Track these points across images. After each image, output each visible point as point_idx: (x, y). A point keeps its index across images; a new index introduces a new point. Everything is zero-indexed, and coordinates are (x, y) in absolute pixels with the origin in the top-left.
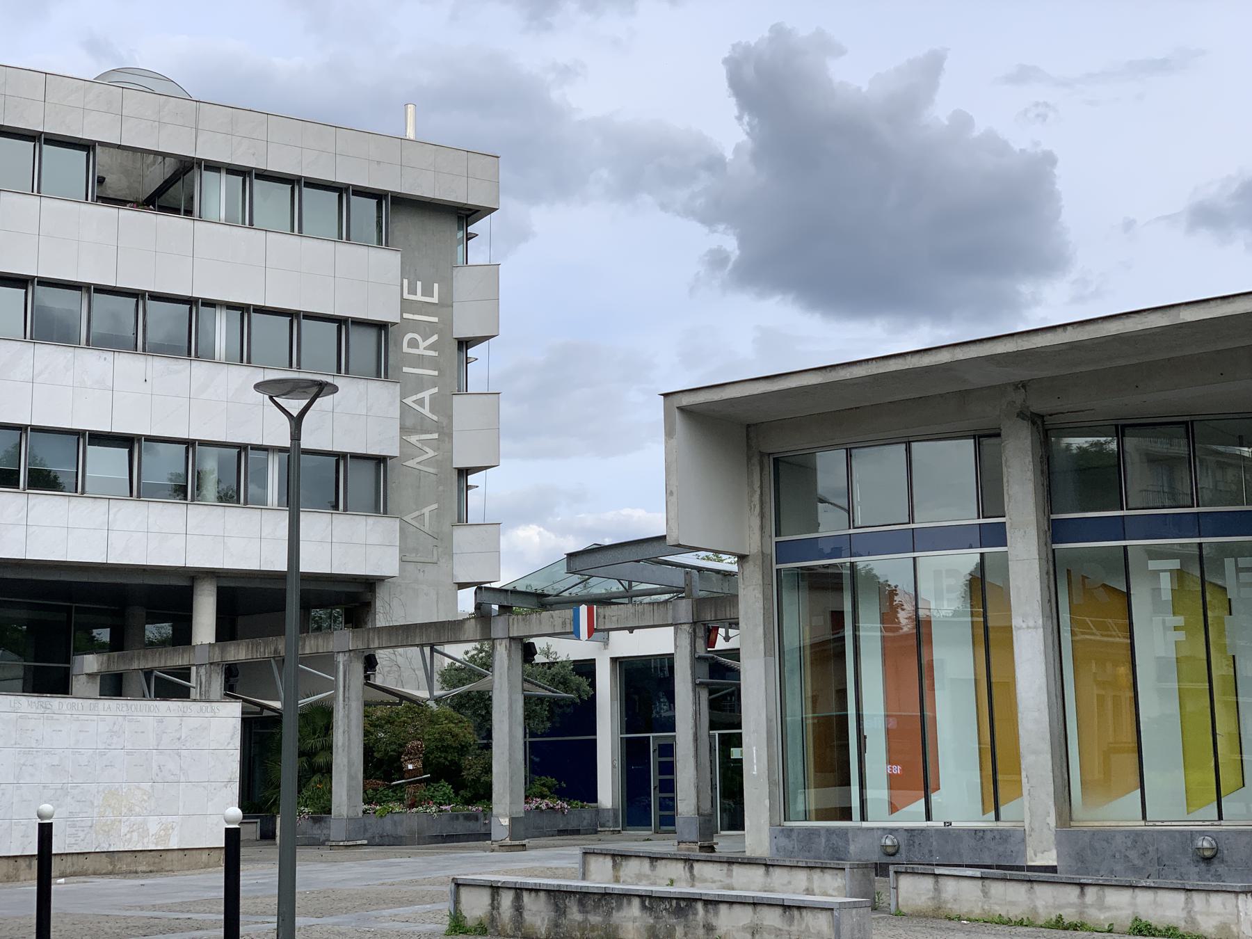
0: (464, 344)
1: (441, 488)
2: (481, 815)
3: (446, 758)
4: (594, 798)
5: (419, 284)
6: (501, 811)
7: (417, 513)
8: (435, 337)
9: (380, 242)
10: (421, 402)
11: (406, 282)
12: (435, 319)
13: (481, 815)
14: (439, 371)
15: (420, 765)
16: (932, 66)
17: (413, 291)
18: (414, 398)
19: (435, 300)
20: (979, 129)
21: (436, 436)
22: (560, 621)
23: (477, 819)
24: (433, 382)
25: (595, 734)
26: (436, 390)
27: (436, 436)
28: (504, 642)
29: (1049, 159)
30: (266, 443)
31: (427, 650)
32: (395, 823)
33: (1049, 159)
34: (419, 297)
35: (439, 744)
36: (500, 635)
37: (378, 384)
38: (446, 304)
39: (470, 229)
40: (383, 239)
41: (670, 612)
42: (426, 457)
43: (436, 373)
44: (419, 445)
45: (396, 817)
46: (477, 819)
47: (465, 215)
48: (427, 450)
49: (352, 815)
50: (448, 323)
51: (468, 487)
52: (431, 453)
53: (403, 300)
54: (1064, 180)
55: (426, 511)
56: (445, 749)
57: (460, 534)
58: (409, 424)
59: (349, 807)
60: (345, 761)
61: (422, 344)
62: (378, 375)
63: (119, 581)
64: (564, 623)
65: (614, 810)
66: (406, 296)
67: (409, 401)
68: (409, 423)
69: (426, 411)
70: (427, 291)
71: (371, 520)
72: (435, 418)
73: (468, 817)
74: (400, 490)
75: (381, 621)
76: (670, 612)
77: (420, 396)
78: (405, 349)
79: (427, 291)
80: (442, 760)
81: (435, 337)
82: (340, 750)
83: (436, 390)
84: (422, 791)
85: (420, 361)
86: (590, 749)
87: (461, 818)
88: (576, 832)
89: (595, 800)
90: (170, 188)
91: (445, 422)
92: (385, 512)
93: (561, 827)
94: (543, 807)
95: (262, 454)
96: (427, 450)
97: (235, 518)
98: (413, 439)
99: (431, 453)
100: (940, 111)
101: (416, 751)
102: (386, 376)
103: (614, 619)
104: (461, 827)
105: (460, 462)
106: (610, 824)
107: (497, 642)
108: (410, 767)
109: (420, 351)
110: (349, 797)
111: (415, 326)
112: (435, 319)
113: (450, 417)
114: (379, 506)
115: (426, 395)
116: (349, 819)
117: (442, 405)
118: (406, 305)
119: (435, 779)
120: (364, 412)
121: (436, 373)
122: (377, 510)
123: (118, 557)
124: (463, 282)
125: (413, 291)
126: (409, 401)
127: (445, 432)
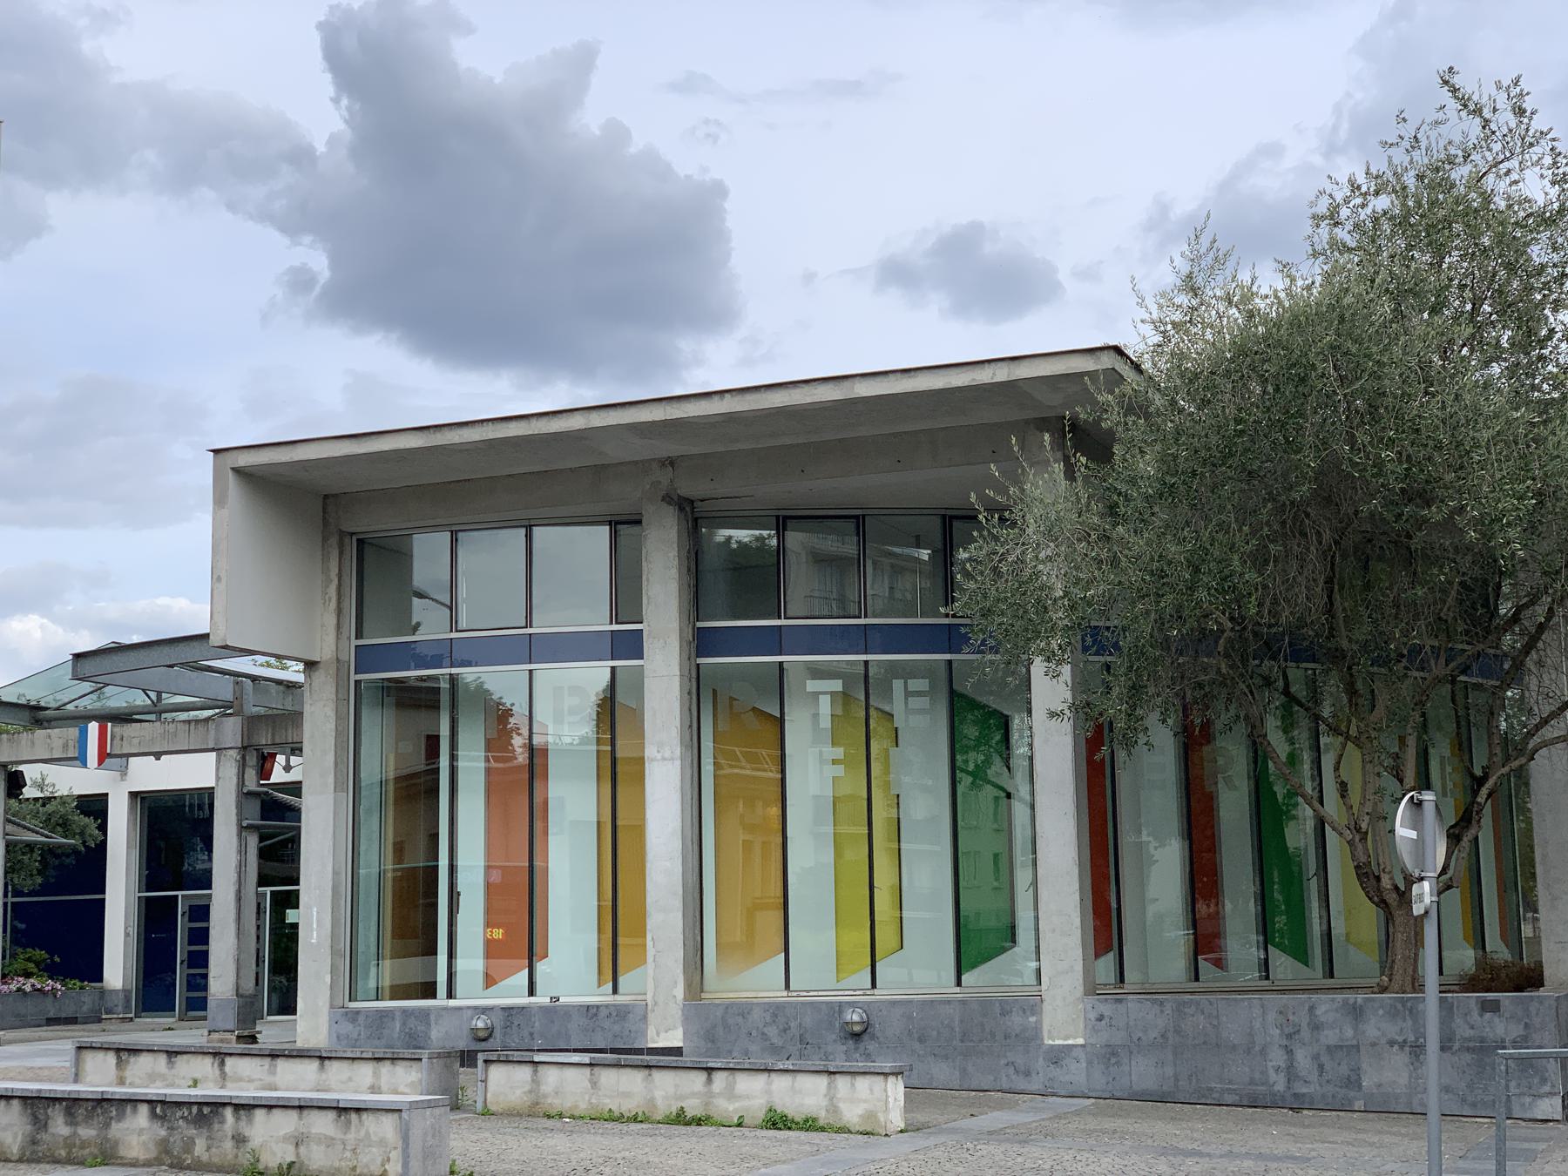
4: (98, 975)
16: (582, 60)
20: (636, 145)
22: (61, 742)
64: (65, 746)
65: (126, 992)
89: (100, 979)
93: (51, 1015)
100: (590, 118)
103: (136, 741)
106: (120, 1009)
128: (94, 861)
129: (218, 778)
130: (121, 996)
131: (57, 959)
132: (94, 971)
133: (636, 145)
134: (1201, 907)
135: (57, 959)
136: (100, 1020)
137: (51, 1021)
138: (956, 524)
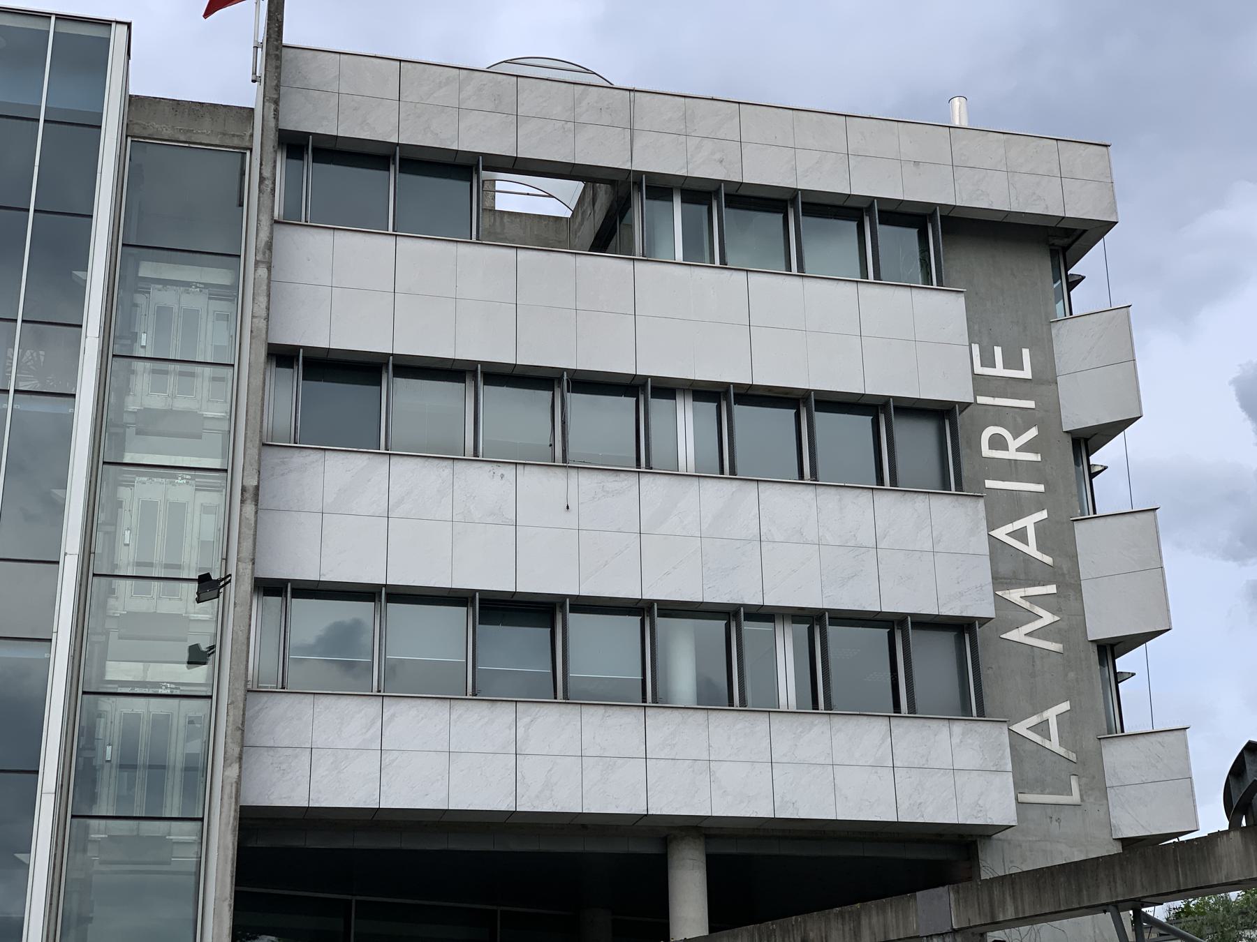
0: (1110, 649)
1: (1072, 675)
5: (998, 351)
7: (1034, 720)
8: (1033, 433)
9: (927, 279)
10: (1021, 535)
11: (976, 348)
12: (1031, 404)
17: (988, 361)
18: (1010, 528)
19: (1027, 373)
21: (1052, 589)
24: (1036, 502)
26: (1043, 515)
27: (1052, 589)
30: (771, 600)
34: (999, 370)
37: (947, 500)
38: (1045, 380)
39: (1094, 459)
40: (930, 275)
42: (1038, 624)
43: (1041, 488)
44: (1026, 605)
47: (1061, 242)
48: (1038, 610)
51: (1119, 677)
52: (1047, 618)
53: (976, 376)
55: (1051, 714)
57: (1115, 756)
58: (1007, 569)
61: (1013, 444)
62: (946, 485)
63: (544, 847)
66: (979, 370)
67: (1001, 533)
68: (1005, 568)
69: (1031, 549)
70: (1013, 361)
71: (958, 728)
72: (1048, 560)
74: (1002, 682)
75: (985, 875)
77: (1018, 525)
78: (986, 452)
79: (1013, 361)
81: (1033, 433)
83: (1043, 515)
85: (1011, 470)
90: (615, 209)
91: (1065, 566)
92: (981, 712)
95: (765, 627)
96: (1038, 610)
97: (730, 732)
98: (1015, 595)
99: (1047, 618)
102: (959, 486)
105: (1100, 630)
109: (1011, 454)
112: (1031, 404)
113: (1074, 558)
114: (971, 702)
115: (1029, 522)
117: (1057, 537)
118: (981, 384)
120: (928, 546)
121: (1041, 488)
122: (965, 710)
123: (535, 801)
124: (1070, 343)
125: (988, 361)
126: (1001, 533)
127: (1068, 581)
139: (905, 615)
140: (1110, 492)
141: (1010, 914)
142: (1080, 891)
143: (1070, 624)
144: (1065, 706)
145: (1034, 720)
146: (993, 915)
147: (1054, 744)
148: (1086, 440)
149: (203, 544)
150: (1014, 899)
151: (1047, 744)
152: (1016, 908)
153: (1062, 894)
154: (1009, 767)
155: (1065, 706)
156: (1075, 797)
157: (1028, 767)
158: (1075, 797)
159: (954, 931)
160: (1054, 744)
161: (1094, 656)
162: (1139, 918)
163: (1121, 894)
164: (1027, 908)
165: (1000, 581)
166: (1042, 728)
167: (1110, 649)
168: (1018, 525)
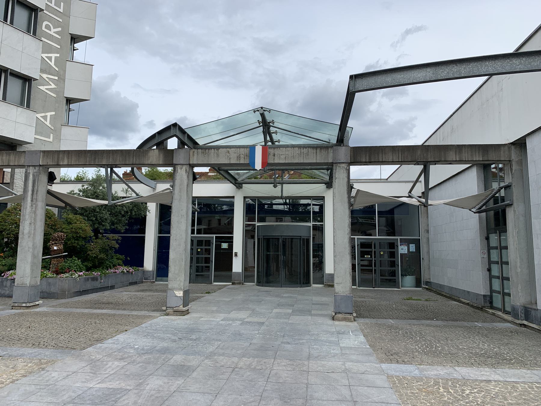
0: (75, 39)
1: (57, 105)
2: (99, 278)
3: (78, 244)
4: (142, 265)
6: (176, 286)
7: (43, 114)
8: (60, 29)
10: (50, 58)
12: (61, 20)
13: (99, 278)
14: (61, 46)
15: (61, 247)
16: (114, 78)
20: (122, 96)
21: (56, 78)
22: (236, 155)
23: (97, 280)
24: (56, 51)
25: (144, 233)
27: (56, 78)
28: (184, 167)
29: (134, 106)
31: (109, 169)
32: (49, 284)
33: (134, 106)
34: (53, 5)
35: (75, 235)
36: (182, 162)
38: (66, 15)
41: (331, 155)
43: (59, 47)
44: (47, 80)
45: (50, 280)
46: (97, 280)
49: (33, 283)
50: (65, 26)
52: (53, 86)
54: (139, 111)
55: (49, 114)
56: (77, 238)
58: (45, 68)
59: (31, 278)
60: (30, 244)
64: (239, 158)
65: (153, 271)
69: (52, 64)
70: (57, 4)
71: (20, 109)
72: (57, 69)
73: (94, 279)
76: (331, 155)
77: (49, 55)
78: (44, 28)
80: (75, 245)
81: (60, 29)
82: (26, 237)
83: (58, 55)
84: (63, 264)
85: (50, 37)
86: (142, 241)
87: (90, 280)
88: (135, 283)
89: (142, 266)
93: (131, 281)
94: (125, 271)
98: (45, 76)
99: (53, 86)
100: (114, 89)
101: (61, 238)
103: (282, 157)
104: (89, 285)
106: (151, 278)
107: (178, 167)
108: (55, 248)
109: (51, 33)
110: (32, 270)
111: (50, 19)
115: (53, 56)
116: (32, 287)
119: (70, 256)
120: (21, 49)
121: (59, 47)
127: (61, 79)
128: (142, 222)
129: (349, 170)
130: (152, 273)
131: (129, 259)
132: (140, 263)
133: (122, 96)
134: (494, 239)
135: (129, 259)
136: (142, 282)
137: (131, 284)
138: (270, 161)
139: (8, 69)
140: (78, 56)
141: (66, 162)
142: (95, 159)
143: (59, 91)
144: (53, 113)
145: (43, 114)
146: (58, 162)
147: (48, 123)
148: (74, 39)
149: (95, 366)
150: (68, 158)
151: (45, 122)
152: (68, 161)
153: (88, 159)
154: (35, 126)
155: (53, 113)
156: (51, 140)
157: (40, 128)
158: (51, 140)
159: (40, 165)
160: (48, 123)
161: (65, 101)
162: (112, 171)
163: (111, 162)
164: (73, 162)
165: (42, 71)
166: (45, 118)
167: (69, 101)
168: (49, 55)
